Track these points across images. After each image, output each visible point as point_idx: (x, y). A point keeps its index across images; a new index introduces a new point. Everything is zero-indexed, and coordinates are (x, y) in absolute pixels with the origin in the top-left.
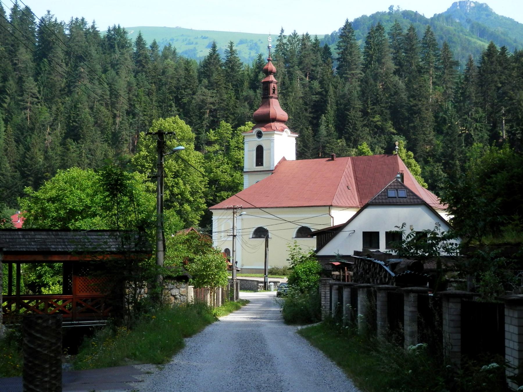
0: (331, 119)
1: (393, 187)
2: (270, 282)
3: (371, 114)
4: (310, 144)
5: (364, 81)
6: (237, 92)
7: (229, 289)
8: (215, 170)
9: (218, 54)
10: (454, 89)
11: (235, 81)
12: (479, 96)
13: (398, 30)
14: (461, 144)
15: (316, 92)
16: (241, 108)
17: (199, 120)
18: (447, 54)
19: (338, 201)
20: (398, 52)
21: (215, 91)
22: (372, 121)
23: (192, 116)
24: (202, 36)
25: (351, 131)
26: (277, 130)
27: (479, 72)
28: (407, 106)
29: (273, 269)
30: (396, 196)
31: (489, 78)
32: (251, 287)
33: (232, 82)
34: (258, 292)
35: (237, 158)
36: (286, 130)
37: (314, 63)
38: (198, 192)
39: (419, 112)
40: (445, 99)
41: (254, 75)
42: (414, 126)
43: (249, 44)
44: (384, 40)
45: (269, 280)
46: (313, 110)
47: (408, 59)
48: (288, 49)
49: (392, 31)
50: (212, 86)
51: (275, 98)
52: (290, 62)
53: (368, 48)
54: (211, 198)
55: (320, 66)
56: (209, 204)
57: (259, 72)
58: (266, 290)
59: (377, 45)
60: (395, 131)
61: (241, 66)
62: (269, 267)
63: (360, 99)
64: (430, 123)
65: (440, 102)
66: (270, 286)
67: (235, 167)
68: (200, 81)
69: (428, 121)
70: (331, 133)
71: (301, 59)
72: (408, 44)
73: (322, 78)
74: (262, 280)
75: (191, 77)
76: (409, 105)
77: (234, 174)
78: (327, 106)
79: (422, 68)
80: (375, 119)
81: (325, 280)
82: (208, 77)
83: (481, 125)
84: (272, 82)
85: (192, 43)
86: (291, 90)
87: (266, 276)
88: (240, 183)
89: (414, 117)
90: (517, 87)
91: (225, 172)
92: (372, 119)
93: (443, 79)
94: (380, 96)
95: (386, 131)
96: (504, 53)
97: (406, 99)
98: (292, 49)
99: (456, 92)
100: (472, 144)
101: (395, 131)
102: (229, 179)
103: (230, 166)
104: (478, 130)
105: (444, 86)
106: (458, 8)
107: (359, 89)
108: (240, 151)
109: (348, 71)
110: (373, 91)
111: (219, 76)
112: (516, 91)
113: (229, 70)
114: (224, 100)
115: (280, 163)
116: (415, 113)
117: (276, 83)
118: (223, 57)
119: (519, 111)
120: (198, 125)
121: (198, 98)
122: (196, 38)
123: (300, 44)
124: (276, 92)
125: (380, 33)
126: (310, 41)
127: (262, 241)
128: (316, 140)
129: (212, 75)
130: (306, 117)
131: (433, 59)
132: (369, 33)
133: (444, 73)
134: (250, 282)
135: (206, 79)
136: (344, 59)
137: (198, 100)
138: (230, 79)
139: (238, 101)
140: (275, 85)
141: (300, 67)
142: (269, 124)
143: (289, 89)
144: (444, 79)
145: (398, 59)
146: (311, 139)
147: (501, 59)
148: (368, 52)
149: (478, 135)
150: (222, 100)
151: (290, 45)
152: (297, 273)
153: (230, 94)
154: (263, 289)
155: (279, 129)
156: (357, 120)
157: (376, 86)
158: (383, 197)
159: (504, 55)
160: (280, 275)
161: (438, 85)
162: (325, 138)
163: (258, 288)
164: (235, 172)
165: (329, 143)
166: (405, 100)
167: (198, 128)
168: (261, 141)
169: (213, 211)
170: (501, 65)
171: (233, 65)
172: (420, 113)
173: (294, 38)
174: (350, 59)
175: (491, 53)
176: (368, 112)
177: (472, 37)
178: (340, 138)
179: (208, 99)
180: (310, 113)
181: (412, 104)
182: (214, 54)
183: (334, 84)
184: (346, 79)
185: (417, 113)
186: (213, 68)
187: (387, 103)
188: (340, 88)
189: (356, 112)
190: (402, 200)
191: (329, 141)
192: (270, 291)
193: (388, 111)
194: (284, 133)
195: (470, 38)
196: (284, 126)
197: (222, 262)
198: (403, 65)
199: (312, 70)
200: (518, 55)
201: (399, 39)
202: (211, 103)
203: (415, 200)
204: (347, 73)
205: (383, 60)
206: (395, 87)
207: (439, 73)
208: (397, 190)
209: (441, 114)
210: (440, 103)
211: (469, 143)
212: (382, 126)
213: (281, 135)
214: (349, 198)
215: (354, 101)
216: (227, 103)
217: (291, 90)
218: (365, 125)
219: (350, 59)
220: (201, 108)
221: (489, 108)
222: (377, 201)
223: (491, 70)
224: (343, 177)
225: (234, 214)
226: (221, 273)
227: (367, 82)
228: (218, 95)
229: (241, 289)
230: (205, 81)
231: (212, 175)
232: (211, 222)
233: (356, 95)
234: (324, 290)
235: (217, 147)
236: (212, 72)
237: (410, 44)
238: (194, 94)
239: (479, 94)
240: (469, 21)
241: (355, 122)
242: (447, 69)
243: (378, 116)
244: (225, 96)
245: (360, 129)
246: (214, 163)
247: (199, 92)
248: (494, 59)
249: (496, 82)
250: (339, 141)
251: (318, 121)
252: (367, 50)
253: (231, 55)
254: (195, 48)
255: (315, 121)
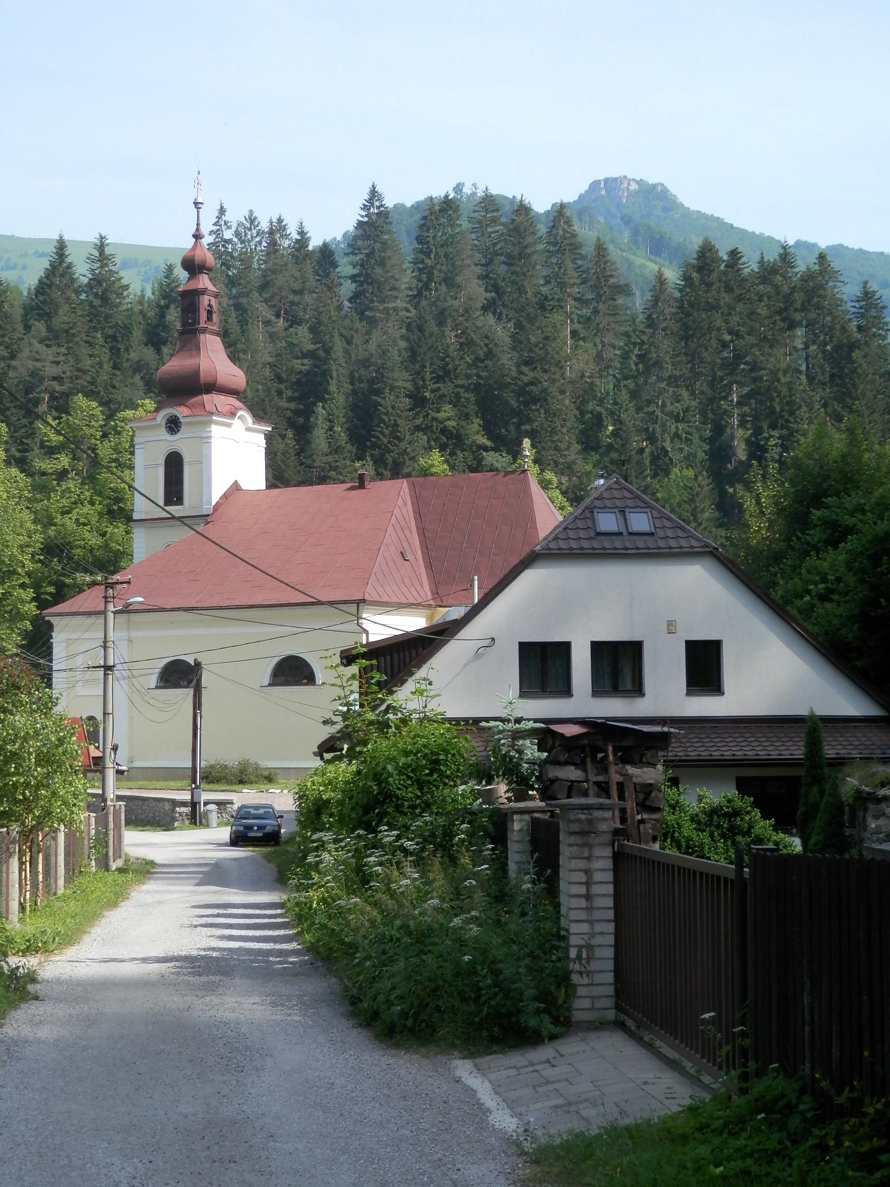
0: (340, 414)
1: (608, 503)
2: (206, 804)
3: (433, 403)
4: (290, 473)
5: (416, 327)
6: (115, 352)
7: (93, 832)
8: (58, 519)
9: (71, 263)
10: (620, 348)
11: (111, 328)
12: (679, 362)
13: (492, 211)
14: (643, 472)
15: (302, 353)
16: (126, 389)
17: (24, 417)
18: (604, 268)
19: (380, 590)
20: (491, 261)
21: (63, 350)
22: (434, 419)
23: (8, 409)
24: (36, 252)
25: (386, 441)
26: (219, 413)
27: (681, 307)
28: (516, 384)
29: (212, 767)
30: (623, 529)
31: (704, 320)
32: (154, 817)
33: (102, 329)
34: (174, 829)
35: (114, 490)
36: (240, 413)
37: (296, 286)
38: (14, 572)
39: (542, 399)
40: (601, 370)
41: (156, 315)
42: (533, 430)
43: (143, 269)
44: (458, 233)
45: (205, 796)
46: (297, 394)
47: (514, 277)
48: (236, 254)
49: (477, 214)
50: (56, 337)
51: (213, 333)
52: (240, 284)
53: (421, 251)
54: (51, 589)
55: (310, 293)
56: (43, 605)
57: (167, 307)
58: (195, 824)
59: (442, 246)
60: (488, 443)
61: (125, 293)
62: (202, 764)
63: (406, 368)
64: (568, 424)
65: (589, 377)
66: (206, 813)
67: (110, 512)
68: (27, 328)
69: (564, 420)
70: (340, 446)
71: (265, 276)
72: (514, 244)
73: (316, 319)
74: (186, 796)
75: (6, 317)
76: (519, 383)
77: (109, 530)
78: (328, 383)
79: (546, 298)
80: (442, 415)
81: (589, 807)
82: (47, 317)
83: (689, 426)
84: (204, 292)
85: (15, 267)
86: (244, 347)
87: (197, 787)
88: (123, 553)
89: (531, 410)
90: (768, 340)
91: (85, 525)
92: (433, 414)
93: (594, 325)
94: (453, 361)
95: (467, 442)
96: (737, 264)
97: (513, 368)
98: (246, 253)
99: (625, 356)
100: (667, 473)
101: (488, 443)
102: (95, 541)
103: (99, 508)
104: (681, 440)
105: (598, 340)
106: (603, 192)
107: (403, 344)
108: (122, 472)
109: (376, 304)
110: (437, 348)
111: (73, 315)
112: (767, 350)
113: (96, 302)
114: (84, 372)
115: (225, 496)
116: (535, 400)
117: (216, 296)
118: (82, 271)
119: (775, 395)
120: (23, 430)
121: (22, 366)
122: (22, 256)
123: (264, 244)
124: (215, 317)
125: (450, 218)
126: (287, 236)
127: (185, 695)
128: (302, 464)
129: (56, 313)
130: (279, 408)
131: (572, 276)
132: (425, 218)
133: (596, 311)
134: (153, 804)
135: (42, 322)
136: (367, 276)
137: (24, 372)
138: (99, 322)
139: (118, 373)
140: (213, 300)
141: (264, 295)
142: (198, 399)
143: (240, 346)
144: (598, 325)
145: (491, 279)
146: (293, 461)
147: (729, 277)
148: (422, 262)
149: (681, 450)
150: (79, 370)
151: (239, 245)
152: (378, 777)
153: (99, 357)
154: (187, 822)
155: (224, 411)
156: (400, 417)
157: (444, 336)
158: (582, 534)
159: (736, 269)
160: (230, 783)
161: (584, 339)
162: (324, 459)
163: (174, 819)
164: (111, 524)
165: (335, 469)
166: (510, 370)
167: (22, 437)
168: (179, 442)
169: (54, 620)
170: (729, 289)
171: (106, 290)
172: (546, 400)
173: (250, 229)
174: (382, 277)
175: (707, 264)
176: (425, 397)
177: (635, 255)
178: (360, 458)
179: (47, 369)
180: (290, 399)
181: (526, 379)
182: (60, 264)
183: (344, 331)
184: (373, 322)
185: (539, 400)
186: (56, 294)
187: (468, 377)
188: (359, 342)
189: (397, 397)
190: (640, 542)
191: (334, 464)
192: (208, 826)
193: (471, 396)
194: (236, 422)
195: (632, 257)
196: (237, 403)
197: (61, 741)
198: (504, 292)
199: (292, 303)
200: (766, 269)
201: (492, 233)
202: (55, 379)
203: (683, 543)
204: (372, 309)
205: (458, 279)
206: (487, 341)
207: (587, 312)
208: (623, 512)
209: (590, 406)
210: (588, 380)
211: (660, 469)
212: (457, 431)
213: (229, 425)
214: (407, 580)
215: (392, 371)
216: (92, 378)
217: (244, 347)
218: (417, 428)
219: (382, 277)
220: (28, 390)
221: (706, 389)
222: (563, 544)
223: (708, 302)
224: (390, 528)
225: (106, 602)
226: (58, 778)
227: (421, 329)
228: (70, 358)
229: (128, 823)
230: (40, 327)
231: (52, 532)
232: (48, 653)
233: (397, 358)
234: (581, 864)
235: (64, 460)
236: (57, 307)
237: (519, 243)
238: (13, 357)
239: (679, 359)
240: (627, 220)
241: (395, 420)
242: (604, 303)
243: (448, 407)
244: (87, 363)
245: (407, 437)
246: (58, 501)
247: (26, 353)
248: (714, 276)
249: (719, 329)
250: (357, 465)
251: (307, 419)
252: (420, 256)
253: (102, 267)
254: (20, 277)
255: (301, 420)
